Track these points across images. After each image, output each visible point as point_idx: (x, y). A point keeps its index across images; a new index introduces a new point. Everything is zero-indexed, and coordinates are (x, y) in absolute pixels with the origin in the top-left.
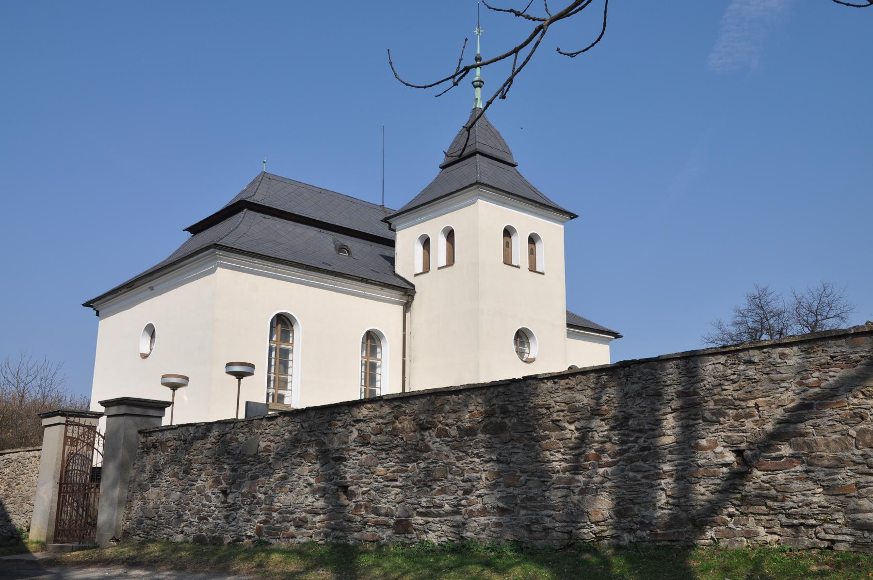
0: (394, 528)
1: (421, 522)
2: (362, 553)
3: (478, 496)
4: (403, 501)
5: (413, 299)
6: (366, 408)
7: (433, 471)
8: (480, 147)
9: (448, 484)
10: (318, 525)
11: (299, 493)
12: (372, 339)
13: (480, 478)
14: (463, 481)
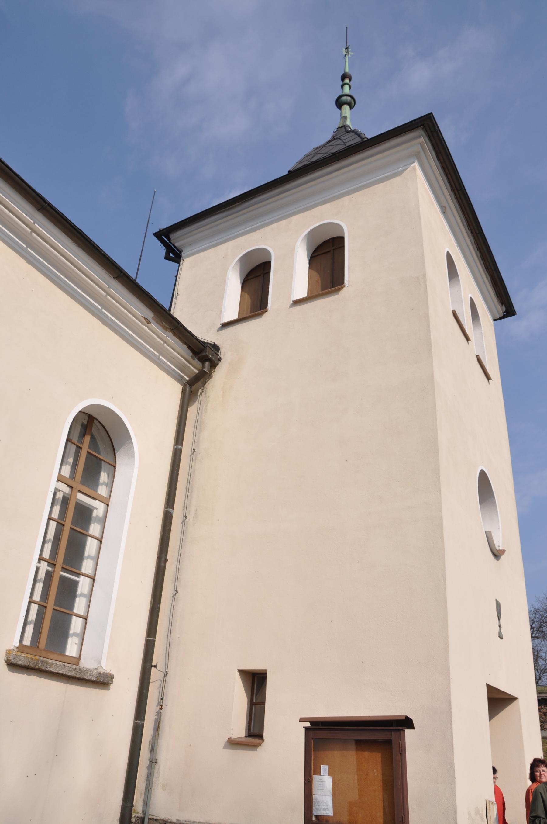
12: (95, 439)
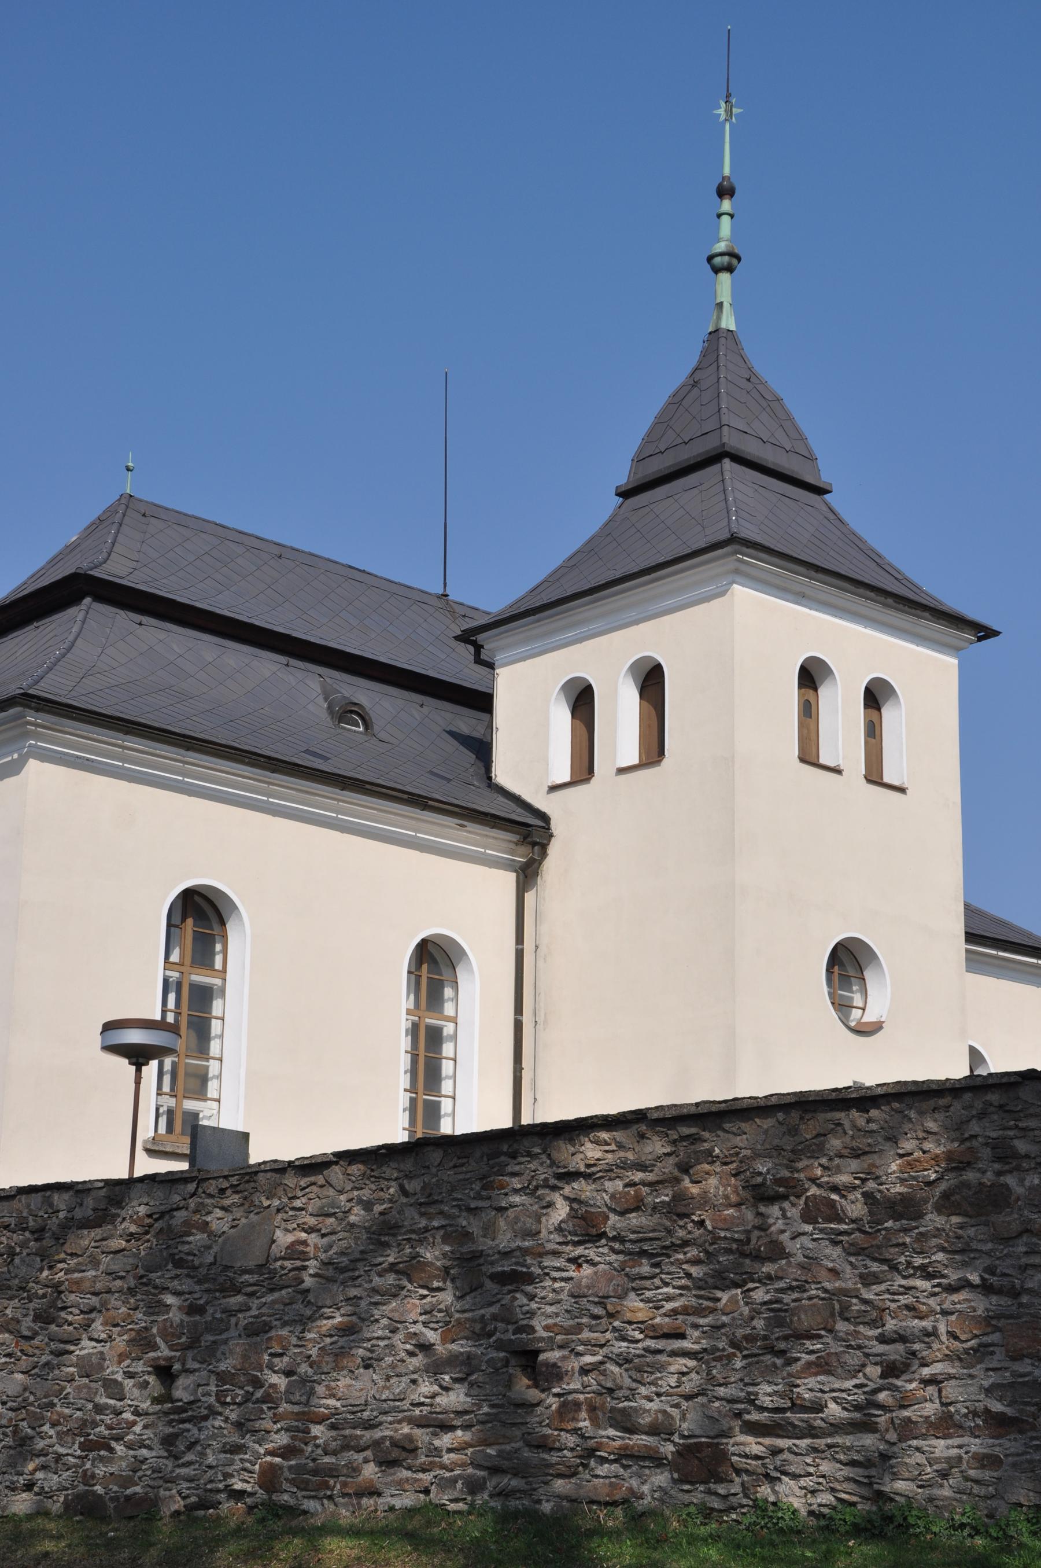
0: (673, 1466)
1: (756, 1449)
2: (591, 1533)
3: (927, 1382)
4: (702, 1393)
5: (544, 854)
6: (598, 1142)
7: (794, 1312)
8: (732, 441)
9: (836, 1348)
11: (400, 1368)
12: (434, 963)
13: (934, 1333)
14: (882, 1339)
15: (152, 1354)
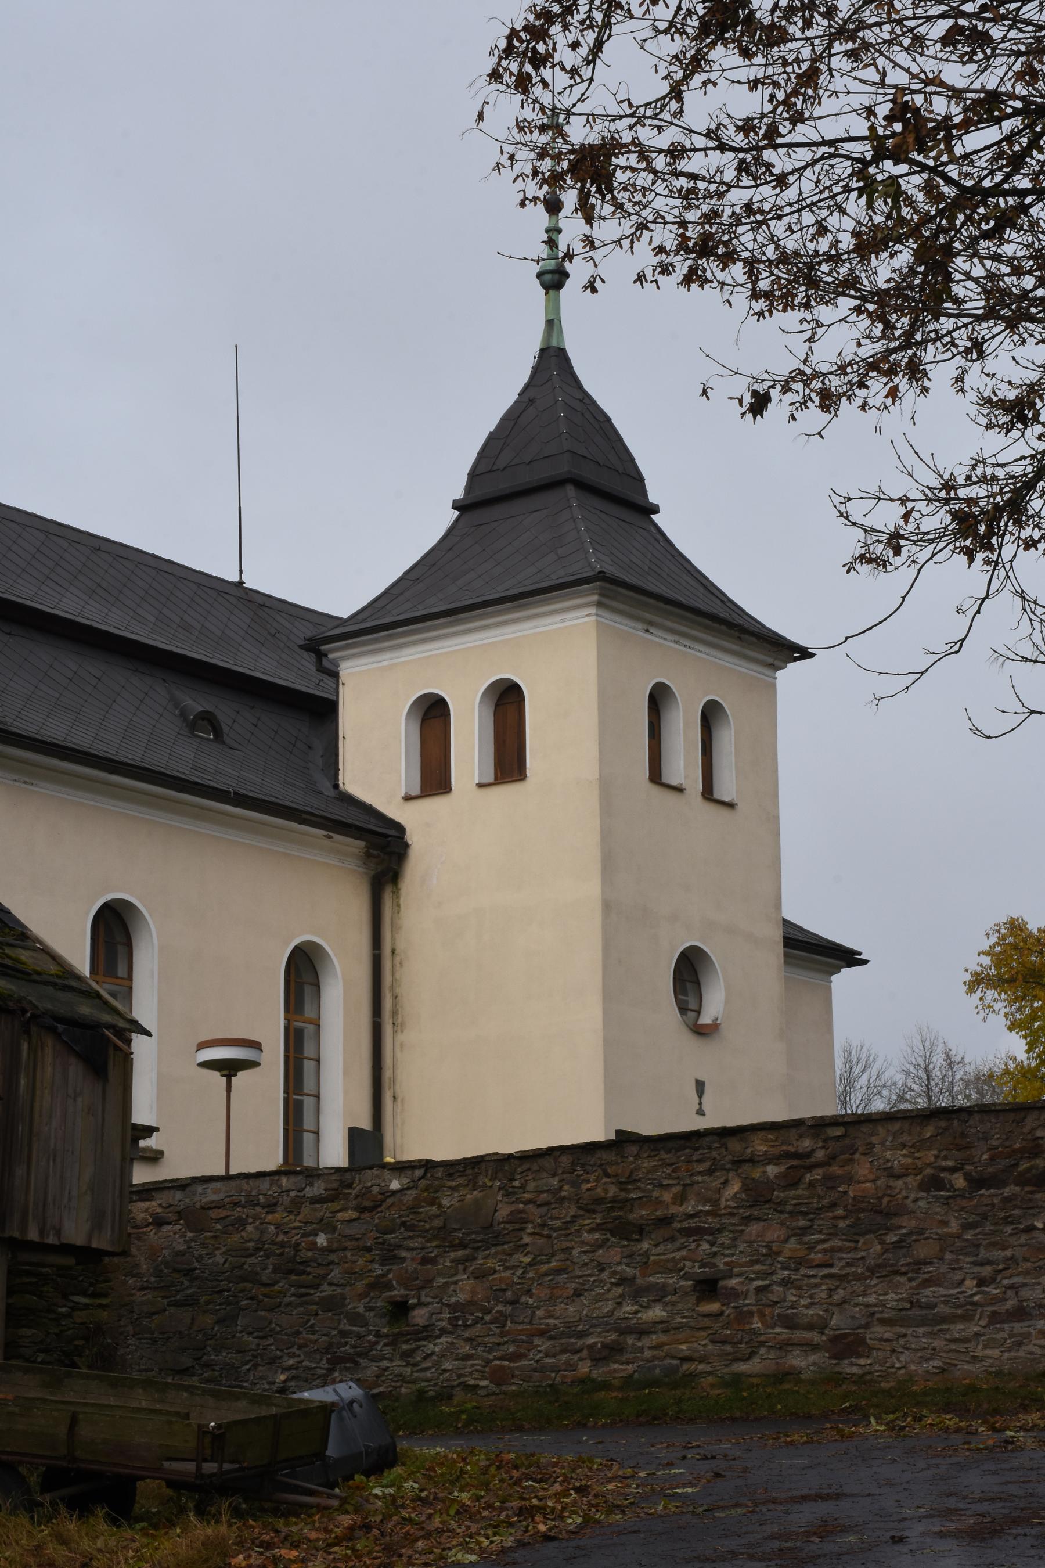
10: (648, 1354)
12: (304, 968)
14: (976, 1264)
15: (389, 1294)
